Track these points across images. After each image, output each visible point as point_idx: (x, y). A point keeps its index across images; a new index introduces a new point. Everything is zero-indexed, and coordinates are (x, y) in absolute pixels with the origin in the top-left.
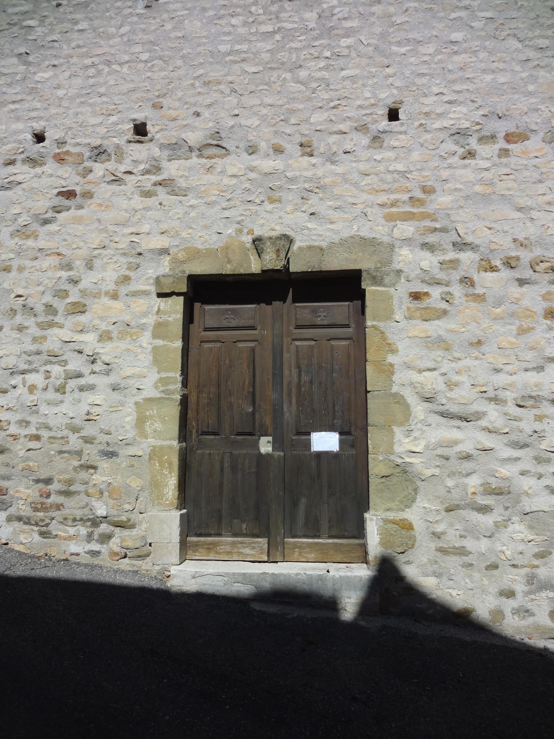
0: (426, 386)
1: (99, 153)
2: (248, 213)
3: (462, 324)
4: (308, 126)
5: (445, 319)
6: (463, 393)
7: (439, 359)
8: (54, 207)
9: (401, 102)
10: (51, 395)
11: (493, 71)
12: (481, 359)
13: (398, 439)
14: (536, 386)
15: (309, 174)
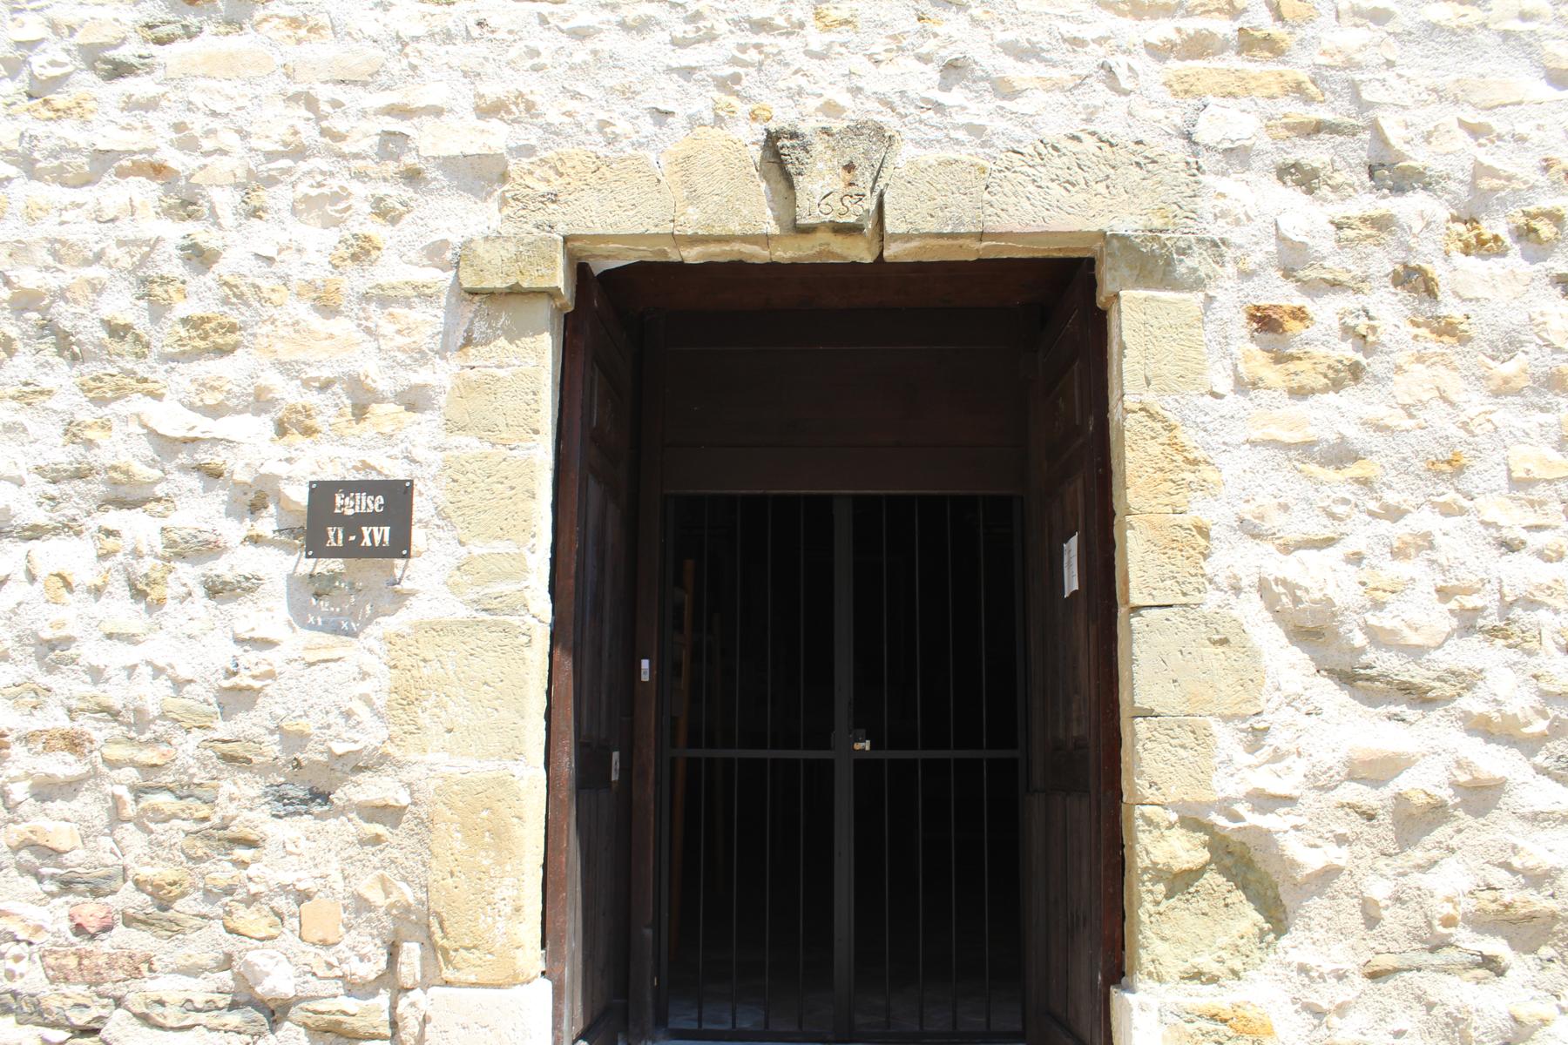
0: (1307, 590)
2: (753, 56)
6: (1416, 616)
7: (1339, 510)
8: (150, 27)
10: (121, 611)
12: (1462, 511)
13: (1223, 757)
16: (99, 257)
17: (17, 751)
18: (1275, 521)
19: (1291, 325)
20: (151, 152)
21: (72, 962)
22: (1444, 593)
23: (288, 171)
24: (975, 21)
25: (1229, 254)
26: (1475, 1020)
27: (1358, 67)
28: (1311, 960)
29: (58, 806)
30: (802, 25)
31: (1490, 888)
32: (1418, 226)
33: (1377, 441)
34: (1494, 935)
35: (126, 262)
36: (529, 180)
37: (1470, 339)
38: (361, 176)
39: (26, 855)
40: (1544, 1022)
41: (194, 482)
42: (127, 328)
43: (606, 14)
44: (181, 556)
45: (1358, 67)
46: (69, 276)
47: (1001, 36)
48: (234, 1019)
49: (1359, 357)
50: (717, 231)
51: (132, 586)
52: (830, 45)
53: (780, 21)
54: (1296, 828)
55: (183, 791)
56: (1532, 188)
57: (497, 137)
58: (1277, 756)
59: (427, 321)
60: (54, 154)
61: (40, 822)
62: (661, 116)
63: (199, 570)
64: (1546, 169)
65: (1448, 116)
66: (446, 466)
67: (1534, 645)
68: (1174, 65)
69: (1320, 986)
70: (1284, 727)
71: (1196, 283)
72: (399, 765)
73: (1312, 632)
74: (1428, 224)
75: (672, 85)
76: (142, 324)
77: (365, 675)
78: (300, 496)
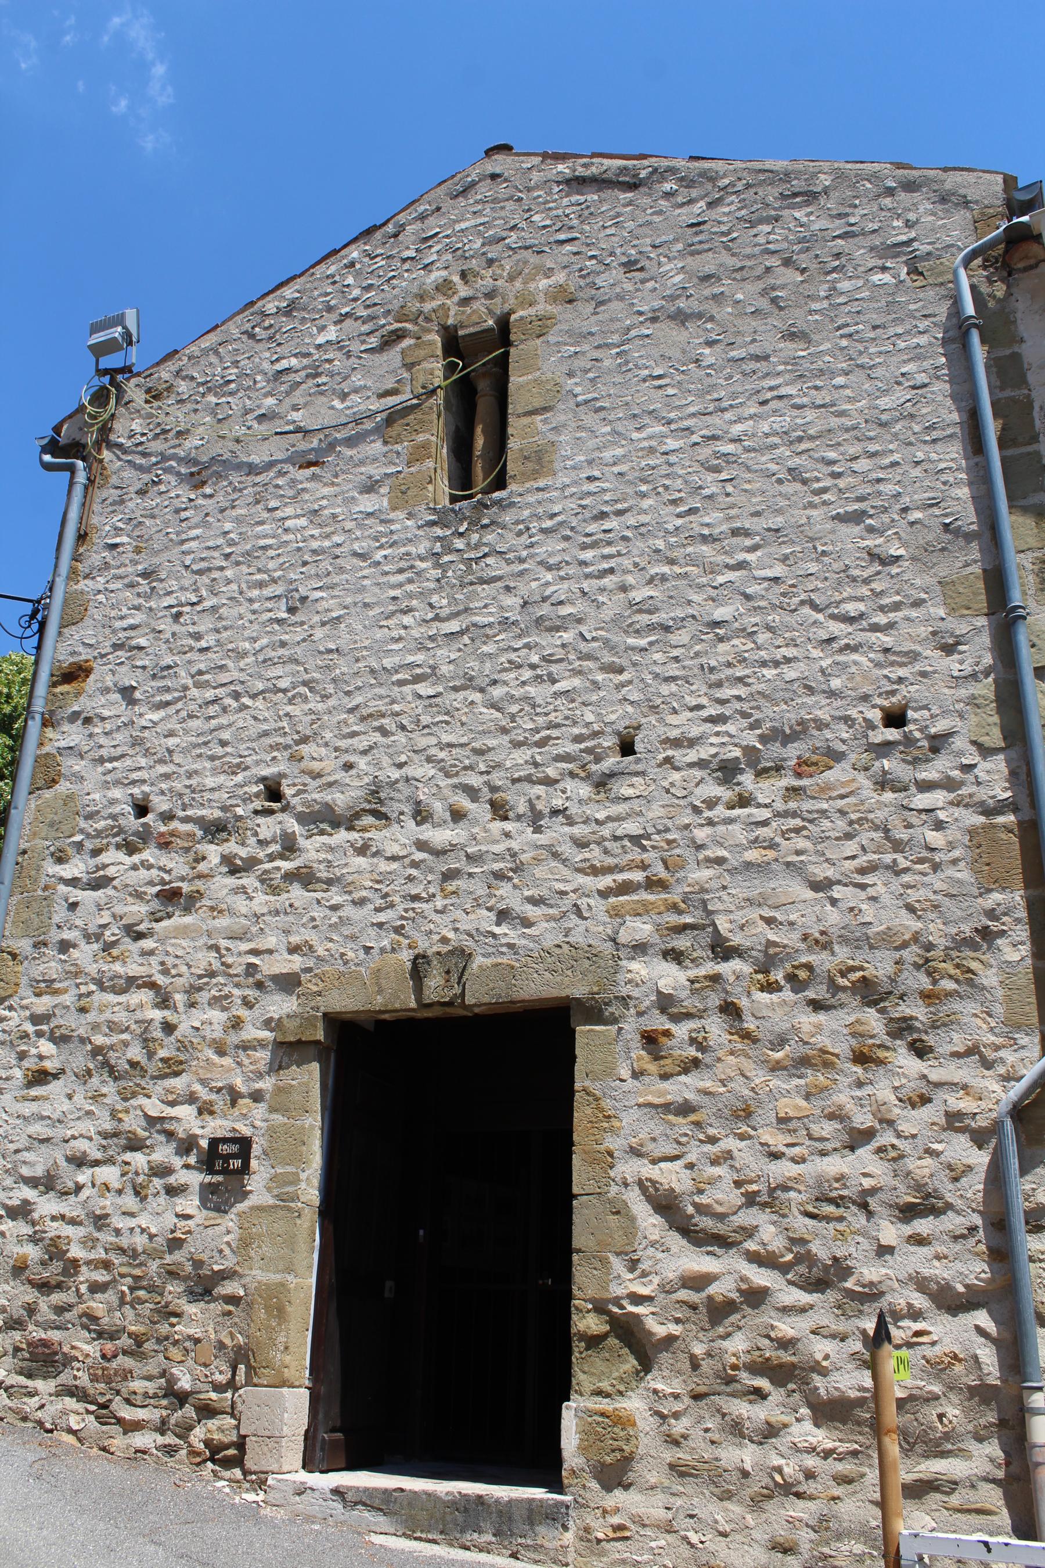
1: (215, 830)
2: (411, 914)
4: (502, 774)
6: (720, 1196)
7: (684, 1139)
8: (153, 913)
9: (638, 727)
10: (129, 1201)
11: (777, 664)
12: (750, 1137)
14: (837, 1180)
15: (498, 848)
16: (127, 1028)
17: (84, 1269)
18: (650, 1147)
19: (663, 1040)
20: (150, 976)
21: (100, 1372)
22: (738, 1184)
23: (207, 984)
24: (515, 887)
25: (632, 1003)
26: (747, 1424)
27: (707, 891)
28: (660, 1386)
29: (98, 1296)
30: (434, 896)
31: (759, 1349)
32: (732, 979)
33: (705, 1100)
34: (762, 1376)
35: (138, 1031)
36: (309, 985)
37: (758, 1040)
38: (237, 985)
39: (84, 1319)
40: (786, 1426)
41: (162, 1138)
42: (138, 1063)
43: (347, 897)
44: (155, 1175)
45: (707, 891)
46: (115, 1038)
47: (527, 893)
48: (164, 1402)
49: (699, 1055)
50: (389, 1007)
51: (134, 1188)
52: (445, 906)
53: (424, 895)
54: (653, 1313)
55: (151, 1289)
56: (797, 951)
57: (297, 963)
58: (644, 1274)
59: (263, 1056)
60: (111, 979)
61: (94, 1305)
62: (368, 949)
63: (162, 1181)
65: (754, 914)
66: (269, 1128)
67: (787, 1211)
68: (612, 900)
69: (664, 1402)
70: (648, 1258)
71: (614, 1020)
72: (241, 1276)
73: (666, 1205)
74: (738, 977)
75: (372, 932)
77: (229, 1232)
78: (204, 1143)
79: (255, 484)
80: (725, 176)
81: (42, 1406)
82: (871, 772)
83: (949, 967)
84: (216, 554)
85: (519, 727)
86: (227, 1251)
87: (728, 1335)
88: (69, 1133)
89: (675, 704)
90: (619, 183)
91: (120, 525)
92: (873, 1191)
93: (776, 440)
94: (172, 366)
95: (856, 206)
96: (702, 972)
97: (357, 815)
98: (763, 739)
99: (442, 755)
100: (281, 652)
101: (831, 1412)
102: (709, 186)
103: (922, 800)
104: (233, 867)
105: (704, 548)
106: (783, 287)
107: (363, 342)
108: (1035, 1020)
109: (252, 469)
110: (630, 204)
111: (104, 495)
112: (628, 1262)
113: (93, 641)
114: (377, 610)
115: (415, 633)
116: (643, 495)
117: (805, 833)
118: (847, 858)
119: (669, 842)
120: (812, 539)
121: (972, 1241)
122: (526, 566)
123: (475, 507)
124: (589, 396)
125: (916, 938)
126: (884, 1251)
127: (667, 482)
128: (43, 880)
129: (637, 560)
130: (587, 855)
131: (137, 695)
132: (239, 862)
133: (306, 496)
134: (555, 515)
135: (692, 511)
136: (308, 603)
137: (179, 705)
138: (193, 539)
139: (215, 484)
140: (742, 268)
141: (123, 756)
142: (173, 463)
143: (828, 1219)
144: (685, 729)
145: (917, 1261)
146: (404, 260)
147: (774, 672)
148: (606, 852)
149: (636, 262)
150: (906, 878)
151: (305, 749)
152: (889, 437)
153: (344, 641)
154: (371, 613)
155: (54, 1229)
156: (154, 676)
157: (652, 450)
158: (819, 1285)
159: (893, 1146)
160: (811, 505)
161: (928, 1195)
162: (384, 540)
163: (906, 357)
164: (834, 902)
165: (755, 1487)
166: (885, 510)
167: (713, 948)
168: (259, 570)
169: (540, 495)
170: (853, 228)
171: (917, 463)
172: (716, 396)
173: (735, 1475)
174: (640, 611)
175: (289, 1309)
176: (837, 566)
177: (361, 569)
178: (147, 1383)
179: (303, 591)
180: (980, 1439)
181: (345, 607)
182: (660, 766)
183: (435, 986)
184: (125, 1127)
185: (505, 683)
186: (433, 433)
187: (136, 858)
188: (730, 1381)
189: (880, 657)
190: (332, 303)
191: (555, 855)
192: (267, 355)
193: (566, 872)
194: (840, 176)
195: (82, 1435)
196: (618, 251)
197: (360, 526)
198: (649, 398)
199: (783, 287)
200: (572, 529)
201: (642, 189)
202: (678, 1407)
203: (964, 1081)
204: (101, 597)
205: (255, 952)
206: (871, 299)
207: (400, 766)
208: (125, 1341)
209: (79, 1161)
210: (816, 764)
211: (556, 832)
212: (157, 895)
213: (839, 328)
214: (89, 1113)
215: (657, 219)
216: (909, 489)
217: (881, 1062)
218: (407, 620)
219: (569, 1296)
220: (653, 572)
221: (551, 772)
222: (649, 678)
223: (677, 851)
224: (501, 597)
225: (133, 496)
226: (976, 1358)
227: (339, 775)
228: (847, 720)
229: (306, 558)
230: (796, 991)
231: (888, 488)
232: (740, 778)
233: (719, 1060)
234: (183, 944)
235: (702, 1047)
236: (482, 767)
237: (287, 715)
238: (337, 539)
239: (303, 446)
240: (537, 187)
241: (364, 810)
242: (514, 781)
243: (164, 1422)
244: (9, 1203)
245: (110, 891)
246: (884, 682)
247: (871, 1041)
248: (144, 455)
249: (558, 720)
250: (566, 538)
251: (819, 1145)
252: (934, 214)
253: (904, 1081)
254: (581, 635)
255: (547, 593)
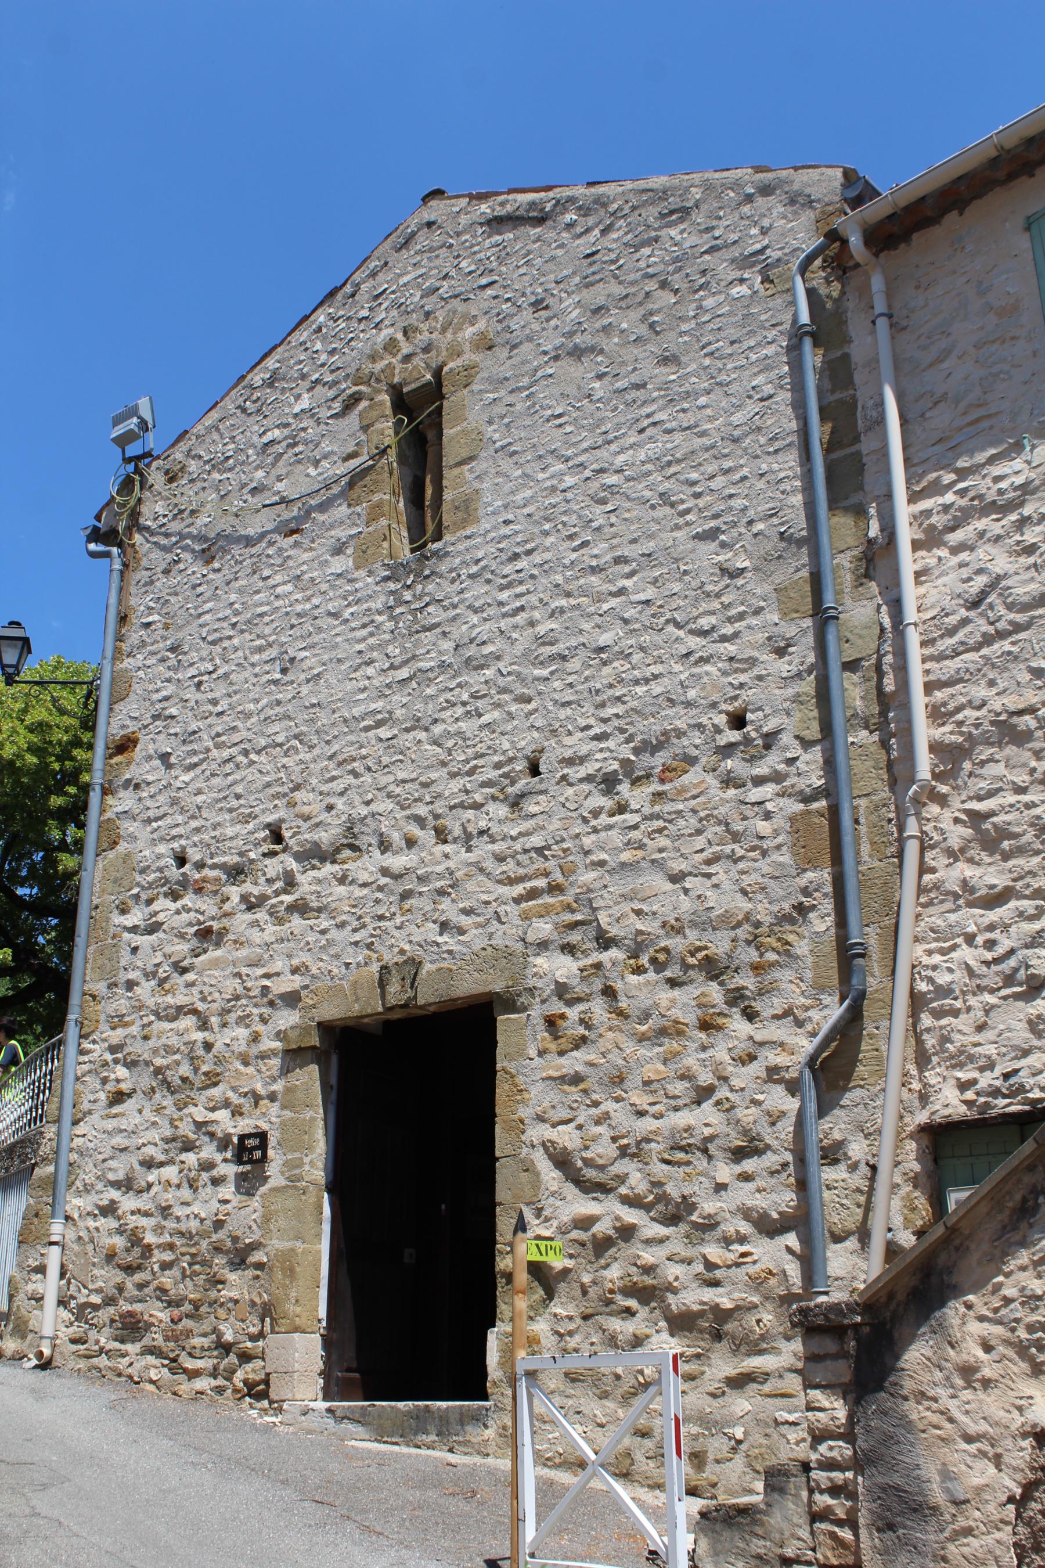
1: (236, 873)
2: (378, 932)
3: (602, 1053)
5: (583, 1049)
6: (600, 1150)
7: (575, 1105)
9: (542, 751)
10: (186, 1193)
12: (623, 1099)
14: (686, 1131)
15: (439, 869)
17: (156, 1252)
19: (560, 1022)
24: (453, 901)
25: (537, 993)
28: (558, 1311)
29: (167, 1272)
32: (609, 965)
38: (256, 1005)
40: (648, 1337)
41: (207, 1139)
47: (461, 906)
48: (215, 1353)
49: (587, 1033)
55: (204, 1263)
58: (547, 1220)
59: (276, 1062)
61: (163, 1280)
62: (347, 965)
64: (664, 927)
65: (626, 907)
68: (524, 905)
70: (549, 1205)
71: (524, 1009)
73: (562, 1161)
75: (350, 950)
76: (191, 1076)
78: (235, 1140)
79: (252, 556)
80: (614, 200)
81: (131, 1364)
82: (717, 773)
83: (772, 941)
84: (225, 625)
85: (454, 759)
86: (254, 1227)
87: (608, 1265)
88: (141, 1141)
89: (570, 727)
90: (529, 218)
91: (151, 604)
92: (711, 1138)
93: (650, 467)
94: (183, 447)
95: (720, 218)
96: (589, 961)
97: (338, 850)
98: (636, 751)
99: (398, 790)
100: (278, 709)
101: (681, 1323)
102: (602, 212)
103: (755, 794)
104: (251, 904)
105: (593, 579)
106: (659, 311)
107: (330, 408)
108: (836, 982)
109: (249, 542)
110: (538, 240)
111: (138, 578)
112: (539, 1219)
113: (136, 715)
114: (348, 664)
115: (376, 682)
116: (546, 534)
117: (666, 832)
118: (697, 852)
119: (565, 851)
120: (677, 560)
121: (784, 1175)
122: (458, 611)
123: (419, 560)
124: (505, 442)
125: (747, 918)
126: (720, 1188)
127: (565, 519)
128: (112, 930)
129: (541, 596)
130: (505, 868)
131: (173, 760)
132: (253, 900)
133: (291, 563)
134: (479, 560)
135: (585, 544)
136: (296, 663)
137: (204, 766)
138: (207, 612)
139: (221, 558)
140: (626, 296)
141: (165, 815)
142: (189, 541)
143: (679, 1164)
144: (576, 748)
145: (744, 1195)
146: (360, 320)
147: (645, 688)
148: (518, 864)
149: (542, 300)
150: (741, 865)
151: (298, 796)
152: (740, 452)
153: (323, 697)
154: (343, 667)
155: (134, 1221)
156: (184, 742)
157: (553, 489)
158: (672, 1220)
159: (727, 1099)
160: (677, 527)
161: (753, 1139)
162: (351, 598)
163: (756, 370)
164: (686, 891)
165: (625, 1387)
166: (735, 524)
167: (597, 939)
168: (258, 636)
169: (469, 543)
170: (718, 242)
171: (762, 475)
172: (604, 429)
173: (611, 1378)
174: (544, 644)
175: (298, 1269)
176: (695, 584)
177: (335, 627)
178: (203, 1339)
179: (291, 653)
180: (788, 1339)
181: (324, 664)
182: (558, 783)
183: (396, 994)
184: (180, 1132)
185: (444, 721)
186: (387, 493)
187: (179, 904)
188: (609, 1302)
189: (725, 666)
190: (305, 370)
191: (482, 870)
192: (256, 428)
193: (489, 884)
194: (708, 187)
195: (159, 1384)
196: (528, 291)
197: (333, 587)
198: (553, 438)
199: (659, 311)
200: (492, 572)
201: (549, 223)
202: (572, 1326)
203: (782, 1039)
204: (141, 674)
205: (267, 976)
206: (731, 313)
207: (368, 803)
208: (187, 1307)
209: (149, 1164)
210: (675, 770)
211: (483, 849)
212: (195, 934)
213: (703, 347)
214: (154, 1123)
215: (560, 252)
216: (755, 501)
217: (720, 1028)
218: (370, 671)
219: (494, 1242)
220: (553, 606)
221: (478, 797)
222: (550, 705)
223: (571, 858)
224: (440, 642)
225: (160, 576)
226: (784, 1272)
227: (324, 816)
228: (700, 726)
229: (294, 621)
230: (657, 972)
231: (738, 503)
232: (619, 788)
233: (601, 1036)
234: (216, 974)
235: (589, 1027)
236: (428, 799)
237: (284, 766)
238: (315, 601)
239: (286, 515)
240: (464, 231)
241: (343, 845)
242: (452, 808)
243: (215, 1368)
244: (101, 1203)
245: (160, 935)
246: (729, 689)
247: (712, 1011)
248: (167, 535)
249: (483, 751)
250: (488, 581)
251: (673, 1102)
252: (785, 217)
253: (736, 1043)
254: (500, 671)
255: (473, 635)
